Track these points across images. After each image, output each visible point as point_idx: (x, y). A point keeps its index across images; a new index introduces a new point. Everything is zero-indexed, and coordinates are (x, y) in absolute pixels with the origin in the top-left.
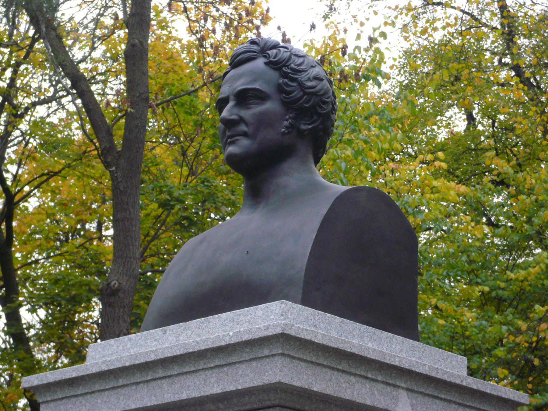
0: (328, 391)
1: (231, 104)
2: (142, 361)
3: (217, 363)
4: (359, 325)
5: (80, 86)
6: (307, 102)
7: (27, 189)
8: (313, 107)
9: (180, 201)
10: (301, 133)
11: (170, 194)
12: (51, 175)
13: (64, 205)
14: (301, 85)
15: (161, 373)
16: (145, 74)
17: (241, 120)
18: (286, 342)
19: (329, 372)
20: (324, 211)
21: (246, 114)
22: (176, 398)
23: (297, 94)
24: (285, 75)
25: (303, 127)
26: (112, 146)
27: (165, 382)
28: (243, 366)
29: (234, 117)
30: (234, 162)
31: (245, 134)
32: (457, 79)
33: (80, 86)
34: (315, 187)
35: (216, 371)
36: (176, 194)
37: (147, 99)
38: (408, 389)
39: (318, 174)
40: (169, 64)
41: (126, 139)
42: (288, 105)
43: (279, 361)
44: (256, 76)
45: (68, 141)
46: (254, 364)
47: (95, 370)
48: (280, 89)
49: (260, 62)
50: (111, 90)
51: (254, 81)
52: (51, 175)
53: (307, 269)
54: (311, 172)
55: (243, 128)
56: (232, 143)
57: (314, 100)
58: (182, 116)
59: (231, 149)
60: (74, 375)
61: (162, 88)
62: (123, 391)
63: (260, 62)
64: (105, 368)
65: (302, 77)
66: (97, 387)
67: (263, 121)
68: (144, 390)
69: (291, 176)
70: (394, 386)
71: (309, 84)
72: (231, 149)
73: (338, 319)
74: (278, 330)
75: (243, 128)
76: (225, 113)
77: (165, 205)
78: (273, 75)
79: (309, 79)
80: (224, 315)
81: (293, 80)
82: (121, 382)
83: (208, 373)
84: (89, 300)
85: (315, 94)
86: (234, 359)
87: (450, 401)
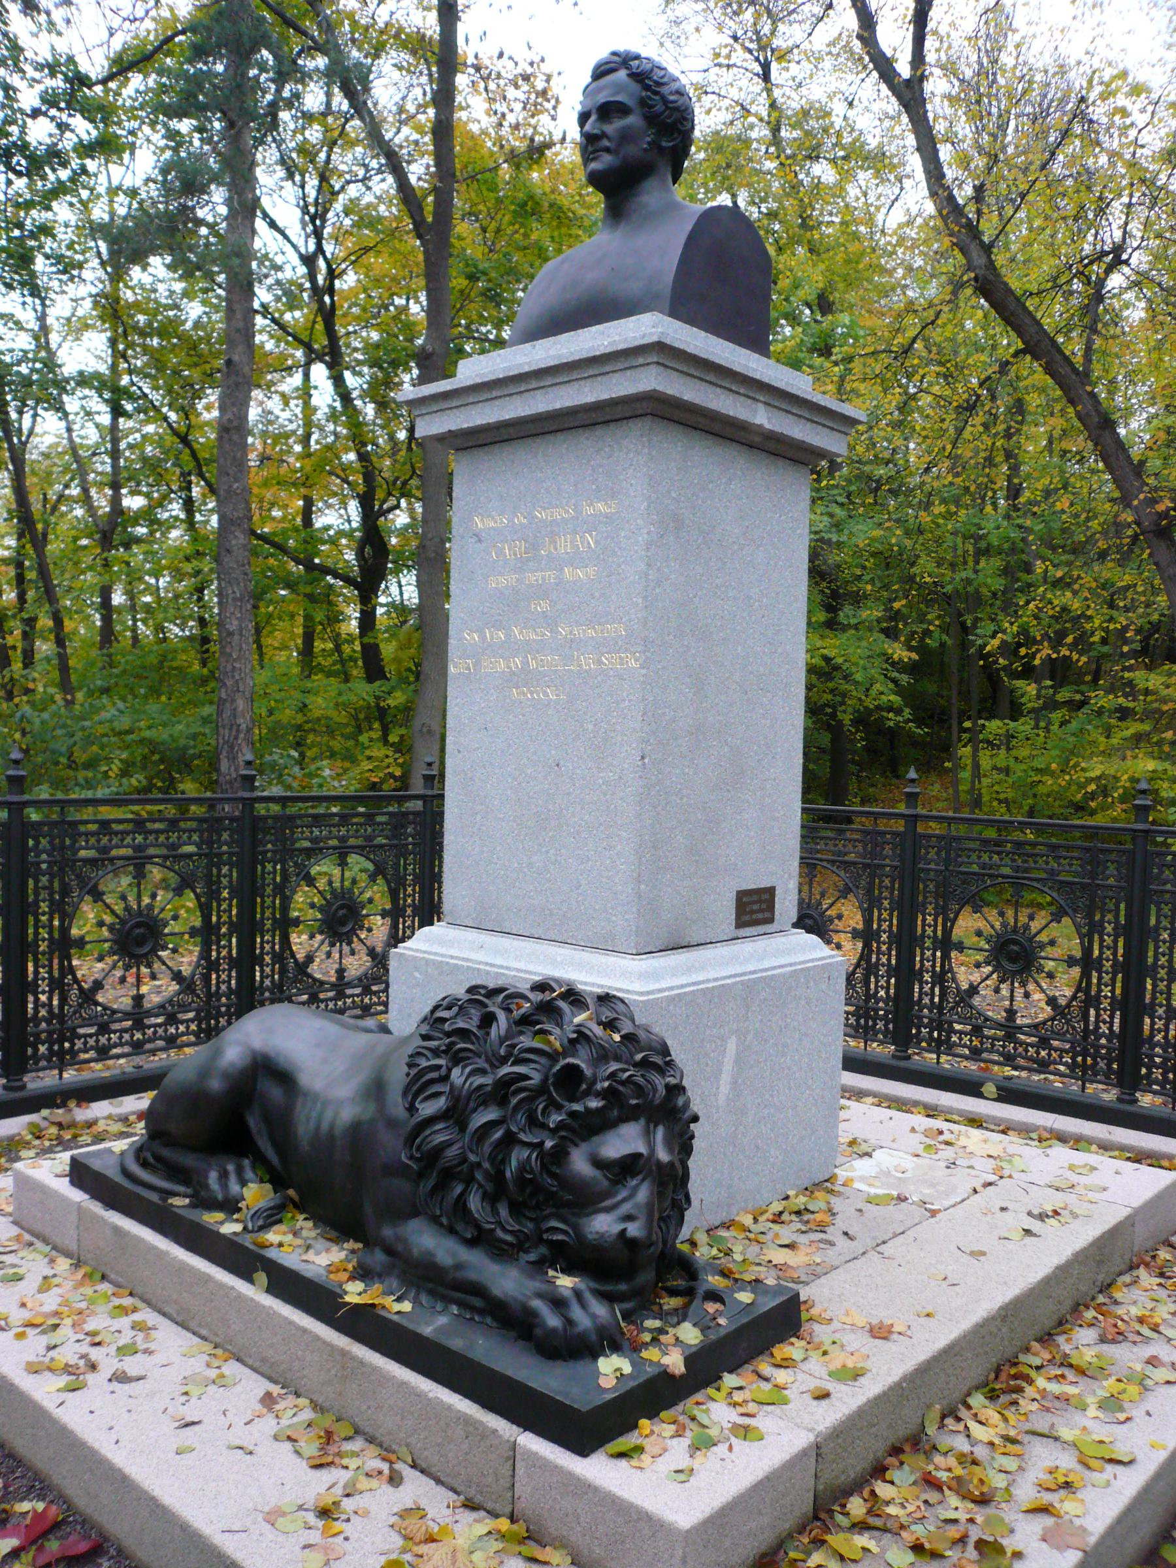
0: (697, 401)
1: (593, 118)
2: (516, 372)
3: (591, 372)
4: (721, 341)
5: (395, 164)
6: (670, 117)
7: (343, 266)
8: (675, 123)
9: (484, 273)
10: (661, 149)
11: (476, 267)
12: (367, 250)
13: (377, 282)
14: (663, 98)
15: (534, 384)
16: (452, 149)
17: (604, 135)
18: (663, 353)
19: (698, 382)
20: (689, 227)
21: (610, 128)
22: (550, 408)
23: (659, 107)
24: (647, 88)
25: (664, 144)
26: (424, 220)
27: (538, 392)
28: (617, 375)
29: (596, 131)
30: (595, 179)
31: (607, 150)
32: (728, 166)
33: (395, 164)
34: (675, 206)
35: (589, 381)
36: (481, 267)
37: (454, 175)
38: (765, 403)
39: (679, 192)
40: (470, 144)
41: (436, 214)
42: (651, 119)
43: (654, 369)
44: (619, 88)
45: (380, 219)
46: (628, 373)
47: (469, 383)
48: (643, 103)
49: (622, 74)
50: (418, 171)
51: (617, 93)
52: (367, 250)
53: (674, 288)
54: (669, 191)
55: (605, 143)
56: (594, 159)
57: (676, 115)
58: (485, 193)
59: (593, 166)
60: (449, 388)
61: (466, 167)
62: (497, 402)
63: (622, 74)
64: (479, 380)
65: (665, 90)
66: (471, 400)
67: (625, 136)
68: (517, 400)
69: (651, 195)
70: (754, 399)
71: (672, 98)
72: (593, 166)
73: (703, 334)
74: (655, 339)
75: (605, 143)
76: (587, 127)
77: (472, 278)
78: (634, 87)
79: (671, 93)
80: (594, 329)
81: (656, 93)
82: (494, 394)
83: (582, 383)
84: (407, 363)
85: (677, 109)
86: (607, 368)
87: (800, 416)
